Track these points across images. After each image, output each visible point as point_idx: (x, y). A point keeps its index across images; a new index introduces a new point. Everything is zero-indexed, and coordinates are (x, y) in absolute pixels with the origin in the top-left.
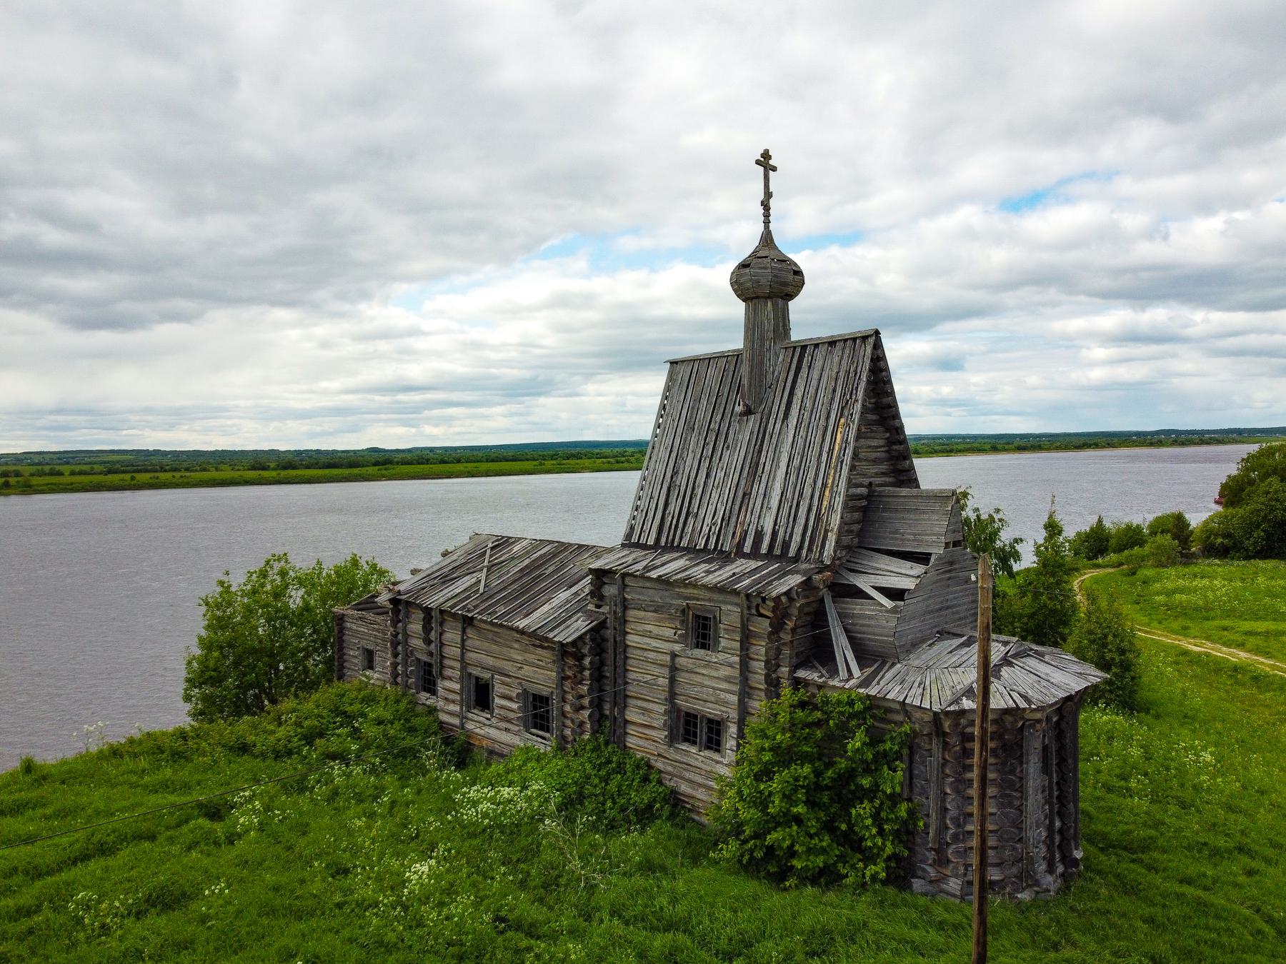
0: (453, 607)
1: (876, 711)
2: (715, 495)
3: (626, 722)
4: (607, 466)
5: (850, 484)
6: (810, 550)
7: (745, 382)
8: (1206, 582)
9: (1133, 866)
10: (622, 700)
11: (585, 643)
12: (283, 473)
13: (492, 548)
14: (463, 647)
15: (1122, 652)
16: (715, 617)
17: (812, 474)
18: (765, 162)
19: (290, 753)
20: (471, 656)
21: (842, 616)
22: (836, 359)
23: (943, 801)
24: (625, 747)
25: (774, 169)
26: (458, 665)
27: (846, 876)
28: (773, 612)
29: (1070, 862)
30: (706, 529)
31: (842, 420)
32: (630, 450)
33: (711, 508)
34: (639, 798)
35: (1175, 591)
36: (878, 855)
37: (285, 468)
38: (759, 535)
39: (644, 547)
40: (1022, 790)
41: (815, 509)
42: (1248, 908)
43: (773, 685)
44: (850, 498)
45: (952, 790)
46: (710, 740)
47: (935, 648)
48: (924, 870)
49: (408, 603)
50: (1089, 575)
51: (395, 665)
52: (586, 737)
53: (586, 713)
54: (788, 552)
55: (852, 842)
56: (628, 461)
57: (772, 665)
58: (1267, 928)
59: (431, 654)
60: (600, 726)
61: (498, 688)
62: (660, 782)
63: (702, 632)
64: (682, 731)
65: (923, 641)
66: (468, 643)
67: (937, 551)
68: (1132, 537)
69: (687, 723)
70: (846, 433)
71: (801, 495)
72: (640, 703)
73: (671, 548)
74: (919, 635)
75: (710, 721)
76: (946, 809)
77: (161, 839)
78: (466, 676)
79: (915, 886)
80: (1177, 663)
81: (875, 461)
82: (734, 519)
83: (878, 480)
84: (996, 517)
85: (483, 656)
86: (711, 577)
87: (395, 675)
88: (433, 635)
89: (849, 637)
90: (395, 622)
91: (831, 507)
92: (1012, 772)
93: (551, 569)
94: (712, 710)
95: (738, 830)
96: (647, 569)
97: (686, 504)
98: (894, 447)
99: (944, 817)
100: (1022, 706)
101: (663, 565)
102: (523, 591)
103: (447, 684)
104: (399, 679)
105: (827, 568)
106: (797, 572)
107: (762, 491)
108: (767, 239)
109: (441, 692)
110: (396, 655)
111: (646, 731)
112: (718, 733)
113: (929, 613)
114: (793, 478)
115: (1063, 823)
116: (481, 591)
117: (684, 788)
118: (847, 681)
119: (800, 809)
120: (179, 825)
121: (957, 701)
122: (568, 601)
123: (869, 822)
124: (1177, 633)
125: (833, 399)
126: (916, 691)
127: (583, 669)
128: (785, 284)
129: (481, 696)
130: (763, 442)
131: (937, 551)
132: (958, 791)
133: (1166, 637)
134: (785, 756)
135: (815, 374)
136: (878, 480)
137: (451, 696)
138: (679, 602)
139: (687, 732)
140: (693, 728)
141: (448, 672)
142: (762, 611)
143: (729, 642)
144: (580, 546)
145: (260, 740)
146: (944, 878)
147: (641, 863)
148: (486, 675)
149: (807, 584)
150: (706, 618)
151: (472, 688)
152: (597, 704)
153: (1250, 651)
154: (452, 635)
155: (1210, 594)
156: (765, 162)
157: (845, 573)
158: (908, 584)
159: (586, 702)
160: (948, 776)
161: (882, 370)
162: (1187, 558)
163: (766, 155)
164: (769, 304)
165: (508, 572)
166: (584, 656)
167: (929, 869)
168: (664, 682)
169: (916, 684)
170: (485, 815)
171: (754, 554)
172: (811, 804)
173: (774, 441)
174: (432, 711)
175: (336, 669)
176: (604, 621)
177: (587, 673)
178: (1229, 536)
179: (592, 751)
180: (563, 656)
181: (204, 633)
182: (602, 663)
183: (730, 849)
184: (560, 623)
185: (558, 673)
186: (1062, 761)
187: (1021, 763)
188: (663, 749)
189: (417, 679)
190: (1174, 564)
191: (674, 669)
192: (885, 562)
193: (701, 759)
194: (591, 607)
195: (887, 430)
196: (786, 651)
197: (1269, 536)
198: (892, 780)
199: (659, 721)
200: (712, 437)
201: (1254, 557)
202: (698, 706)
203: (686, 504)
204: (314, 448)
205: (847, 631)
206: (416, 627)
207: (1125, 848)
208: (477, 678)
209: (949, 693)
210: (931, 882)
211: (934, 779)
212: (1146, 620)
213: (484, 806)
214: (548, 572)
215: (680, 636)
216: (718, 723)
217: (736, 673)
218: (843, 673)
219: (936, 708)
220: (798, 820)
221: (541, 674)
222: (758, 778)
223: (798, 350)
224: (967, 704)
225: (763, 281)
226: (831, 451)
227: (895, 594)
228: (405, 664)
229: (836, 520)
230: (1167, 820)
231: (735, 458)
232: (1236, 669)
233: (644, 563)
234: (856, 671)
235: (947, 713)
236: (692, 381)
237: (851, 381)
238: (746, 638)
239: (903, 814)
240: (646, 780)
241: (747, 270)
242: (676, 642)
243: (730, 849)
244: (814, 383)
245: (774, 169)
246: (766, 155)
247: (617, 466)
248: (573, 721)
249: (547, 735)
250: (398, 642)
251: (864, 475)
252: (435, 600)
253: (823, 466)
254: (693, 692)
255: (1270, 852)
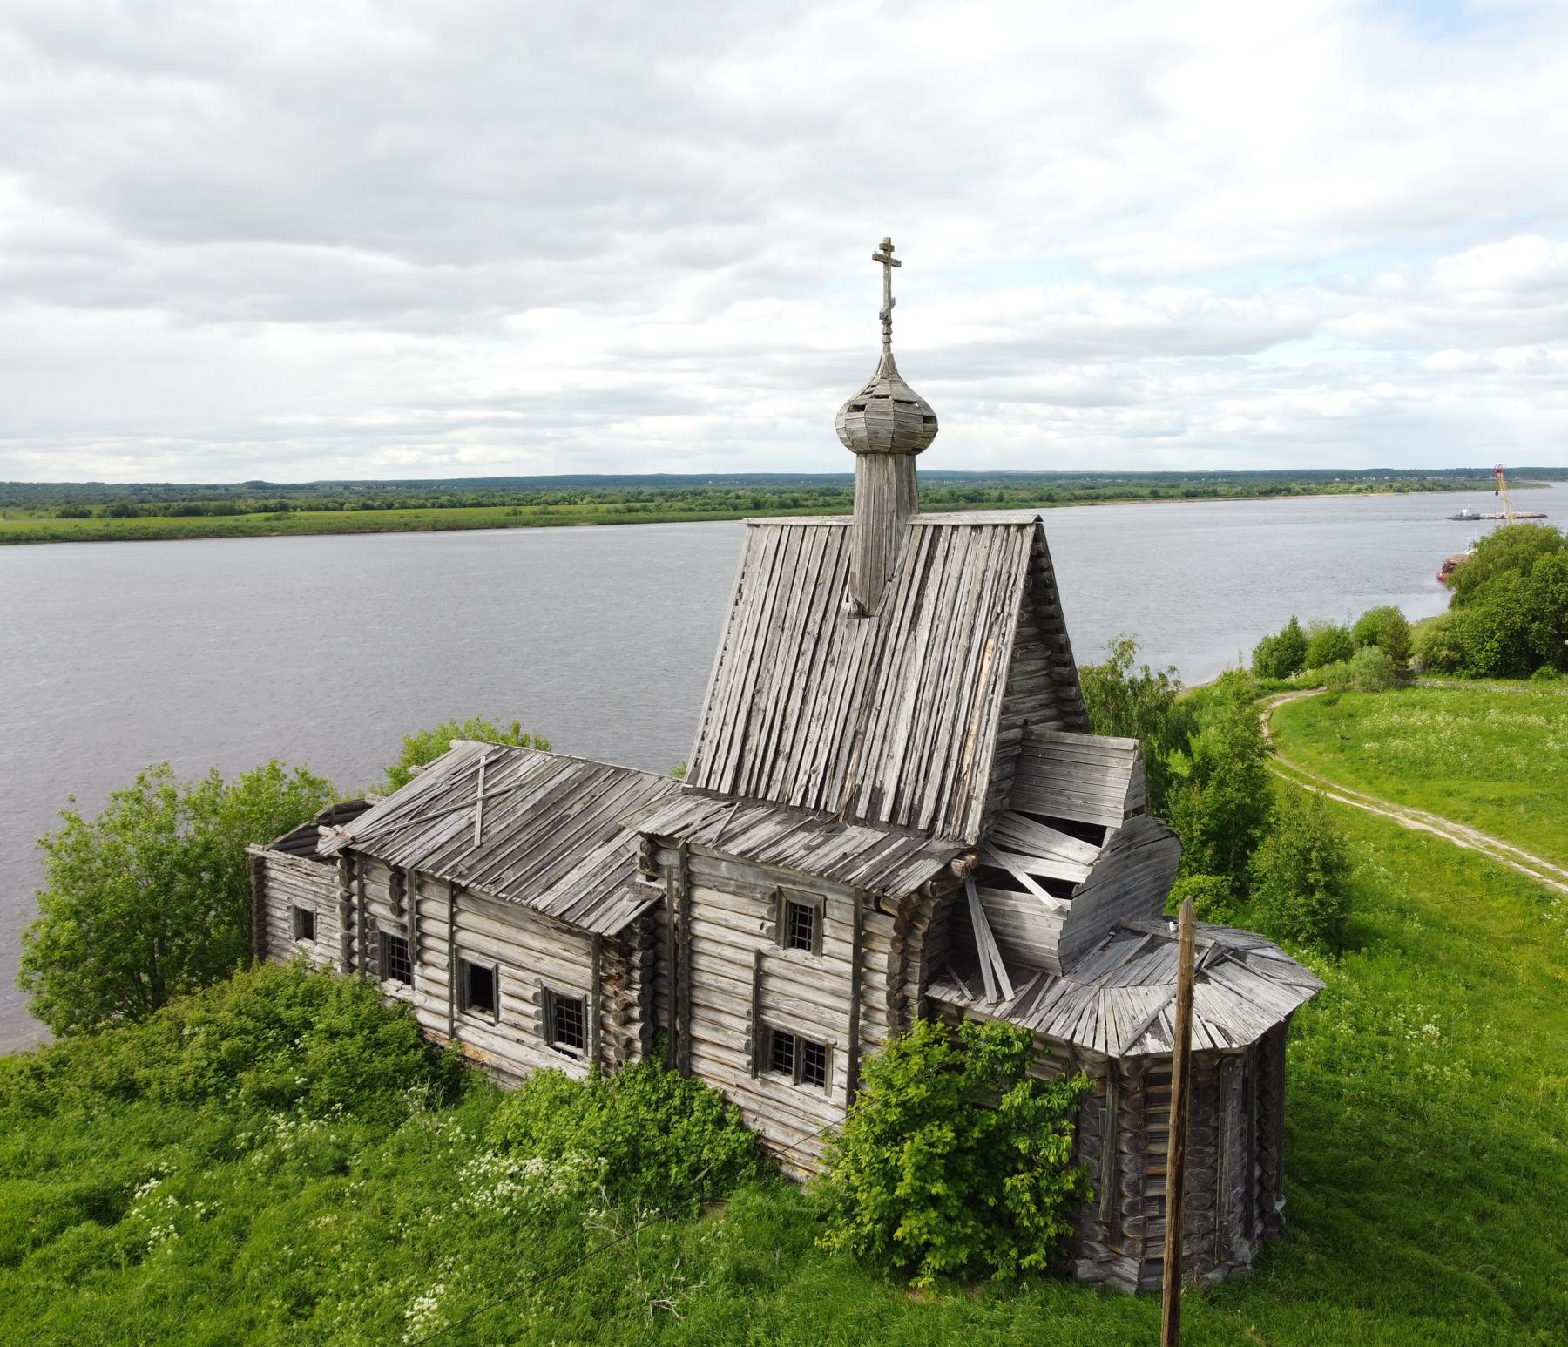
0: (437, 867)
1: (1039, 1047)
2: (816, 730)
3: (694, 1039)
4: (614, 516)
5: (1001, 728)
6: (947, 821)
7: (856, 568)
8: (1425, 716)
9: (1345, 1212)
10: (686, 1008)
11: (634, 933)
12: (116, 524)
13: (487, 766)
14: (452, 921)
15: (1327, 868)
16: (817, 908)
17: (948, 716)
18: (886, 256)
19: (202, 1095)
20: (463, 937)
21: (991, 914)
22: (984, 552)
23: (1118, 1162)
24: (691, 1072)
25: (897, 264)
26: (445, 947)
27: (994, 1269)
28: (899, 910)
29: (1266, 1215)
30: (803, 778)
31: (991, 642)
32: (647, 490)
33: (810, 749)
34: (714, 1154)
35: (1391, 732)
36: (1036, 1237)
37: (117, 514)
38: (877, 795)
39: (716, 796)
40: (1217, 1144)
41: (953, 764)
42: (1480, 1273)
43: (899, 1005)
44: (1001, 745)
45: (1130, 1148)
46: (809, 1070)
47: (1109, 952)
48: (1092, 1249)
49: (364, 856)
50: (1282, 700)
51: (348, 940)
52: (636, 1060)
53: (635, 1029)
54: (917, 823)
55: (1003, 1220)
56: (645, 509)
57: (898, 981)
58: (1503, 1307)
59: (403, 928)
60: (656, 1044)
61: (505, 984)
62: (741, 1126)
63: (799, 926)
64: (770, 1056)
65: (1094, 943)
66: (462, 919)
67: (1112, 819)
68: (1338, 648)
69: (778, 1045)
70: (997, 659)
71: (934, 742)
72: (712, 1015)
73: (752, 800)
74: (1089, 937)
75: (809, 1045)
76: (1122, 1172)
77: (28, 1263)
78: (457, 965)
79: (1080, 1270)
80: (1391, 849)
81: (1032, 691)
82: (841, 768)
83: (1035, 716)
84: (1171, 678)
85: (483, 938)
86: (813, 857)
87: (350, 953)
88: (405, 903)
89: (997, 941)
90: (348, 878)
91: (975, 764)
92: (1205, 1122)
93: (578, 808)
94: (813, 1032)
95: (850, 1209)
96: (725, 838)
97: (774, 739)
98: (1057, 669)
99: (1118, 1184)
100: (1220, 1046)
101: (745, 831)
102: (537, 845)
103: (429, 972)
104: (356, 961)
105: (971, 850)
106: (930, 855)
107: (880, 731)
108: (889, 369)
109: (418, 981)
110: (349, 925)
111: (722, 1058)
112: (822, 1061)
113: (1103, 905)
114: (923, 717)
115: (1264, 1172)
116: (477, 842)
117: (773, 1132)
118: (997, 1004)
119: (938, 1188)
120: (51, 1240)
121: (1138, 1041)
122: (605, 865)
123: (1026, 1197)
124: (1391, 798)
125: (977, 609)
126: (1086, 1024)
127: (631, 968)
128: (913, 436)
129: (477, 988)
130: (880, 664)
131: (1112, 819)
132: (1136, 1149)
133: (1378, 805)
134: (916, 1116)
135: (954, 568)
136: (1035, 716)
137: (435, 989)
138: (768, 883)
139: (778, 1057)
140: (782, 1053)
141: (428, 956)
142: (883, 907)
143: (837, 943)
144: (618, 771)
145: (156, 1071)
146: (1116, 1258)
147: (727, 1273)
148: (488, 964)
149: (945, 874)
150: (804, 908)
151: (467, 979)
152: (650, 1016)
153: (1479, 828)
154: (435, 907)
155: (1432, 738)
156: (886, 256)
157: (993, 851)
158: (1077, 875)
159: (636, 1012)
160: (1125, 1130)
161: (1043, 570)
162: (1403, 678)
163: (888, 247)
164: (891, 462)
165: (513, 810)
166: (631, 951)
167: (1099, 1247)
168: (748, 990)
169: (1087, 1013)
170: (507, 1200)
171: (871, 820)
172: (951, 1175)
173: (897, 660)
174: (405, 1008)
175: (253, 940)
176: (661, 900)
177: (637, 975)
178: (1455, 647)
179: (645, 1081)
180: (601, 948)
181: (48, 890)
182: (657, 958)
183: (838, 1238)
184: (599, 903)
185: (596, 972)
186: (1265, 1092)
187: (1217, 1110)
188: (744, 1079)
189: (383, 961)
190: (1386, 687)
191: (760, 976)
192: (1042, 836)
193: (798, 1095)
194: (641, 879)
195: (1049, 647)
196: (916, 964)
197: (1504, 650)
198: (1056, 1148)
199: (741, 1041)
200: (809, 645)
201: (1485, 676)
202: (793, 1025)
203: (774, 739)
204: (162, 481)
205: (995, 932)
206: (379, 887)
207: (1335, 1184)
208: (474, 967)
209: (1129, 1027)
210: (1101, 1263)
211: (1108, 1136)
212: (1352, 778)
213: (504, 1188)
214: (572, 812)
215: (769, 929)
216: (821, 1049)
217: (847, 987)
218: (991, 995)
219: (1114, 1052)
220: (935, 1201)
221: (573, 973)
222: (879, 1141)
223: (930, 530)
224: (1153, 1045)
225: (883, 432)
226: (975, 684)
227: (1058, 888)
228: (363, 937)
229: (981, 784)
230: (1385, 1137)
231: (843, 678)
232: (1465, 860)
233: (719, 827)
234: (1009, 993)
235: (1125, 1058)
236: (780, 556)
237: (1002, 587)
238: (862, 941)
239: (1070, 1186)
240: (721, 1122)
241: (861, 414)
242: (762, 937)
243: (838, 1238)
244: (953, 582)
245: (897, 264)
246: (888, 247)
247: (628, 516)
248: (617, 1038)
249: (578, 1051)
250: (353, 911)
251: (1018, 712)
252: (409, 853)
253: (965, 704)
254: (787, 1005)
255: (1506, 1181)
